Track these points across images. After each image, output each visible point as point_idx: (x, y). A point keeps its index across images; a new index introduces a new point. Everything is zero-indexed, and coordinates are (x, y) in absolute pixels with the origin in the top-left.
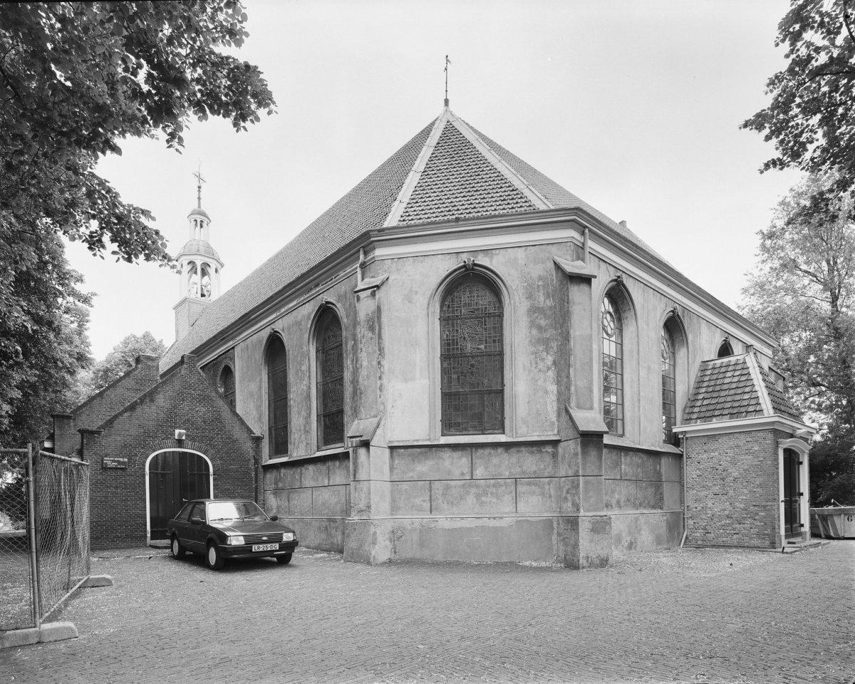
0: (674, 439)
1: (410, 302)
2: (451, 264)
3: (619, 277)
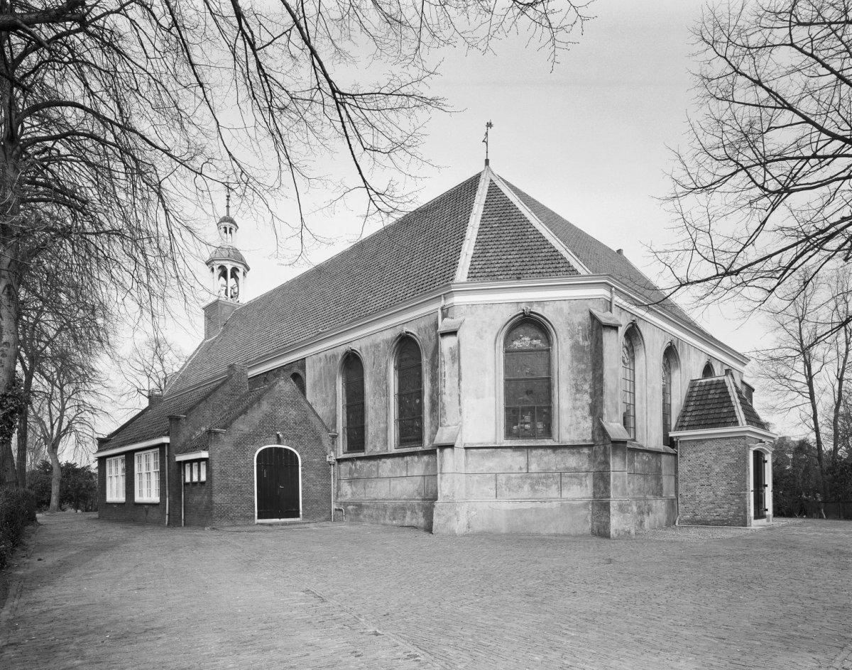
0: (670, 442)
1: (481, 338)
2: (513, 312)
3: (634, 321)
